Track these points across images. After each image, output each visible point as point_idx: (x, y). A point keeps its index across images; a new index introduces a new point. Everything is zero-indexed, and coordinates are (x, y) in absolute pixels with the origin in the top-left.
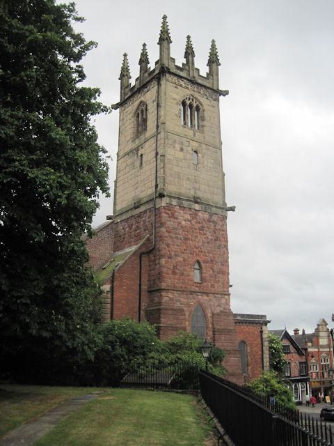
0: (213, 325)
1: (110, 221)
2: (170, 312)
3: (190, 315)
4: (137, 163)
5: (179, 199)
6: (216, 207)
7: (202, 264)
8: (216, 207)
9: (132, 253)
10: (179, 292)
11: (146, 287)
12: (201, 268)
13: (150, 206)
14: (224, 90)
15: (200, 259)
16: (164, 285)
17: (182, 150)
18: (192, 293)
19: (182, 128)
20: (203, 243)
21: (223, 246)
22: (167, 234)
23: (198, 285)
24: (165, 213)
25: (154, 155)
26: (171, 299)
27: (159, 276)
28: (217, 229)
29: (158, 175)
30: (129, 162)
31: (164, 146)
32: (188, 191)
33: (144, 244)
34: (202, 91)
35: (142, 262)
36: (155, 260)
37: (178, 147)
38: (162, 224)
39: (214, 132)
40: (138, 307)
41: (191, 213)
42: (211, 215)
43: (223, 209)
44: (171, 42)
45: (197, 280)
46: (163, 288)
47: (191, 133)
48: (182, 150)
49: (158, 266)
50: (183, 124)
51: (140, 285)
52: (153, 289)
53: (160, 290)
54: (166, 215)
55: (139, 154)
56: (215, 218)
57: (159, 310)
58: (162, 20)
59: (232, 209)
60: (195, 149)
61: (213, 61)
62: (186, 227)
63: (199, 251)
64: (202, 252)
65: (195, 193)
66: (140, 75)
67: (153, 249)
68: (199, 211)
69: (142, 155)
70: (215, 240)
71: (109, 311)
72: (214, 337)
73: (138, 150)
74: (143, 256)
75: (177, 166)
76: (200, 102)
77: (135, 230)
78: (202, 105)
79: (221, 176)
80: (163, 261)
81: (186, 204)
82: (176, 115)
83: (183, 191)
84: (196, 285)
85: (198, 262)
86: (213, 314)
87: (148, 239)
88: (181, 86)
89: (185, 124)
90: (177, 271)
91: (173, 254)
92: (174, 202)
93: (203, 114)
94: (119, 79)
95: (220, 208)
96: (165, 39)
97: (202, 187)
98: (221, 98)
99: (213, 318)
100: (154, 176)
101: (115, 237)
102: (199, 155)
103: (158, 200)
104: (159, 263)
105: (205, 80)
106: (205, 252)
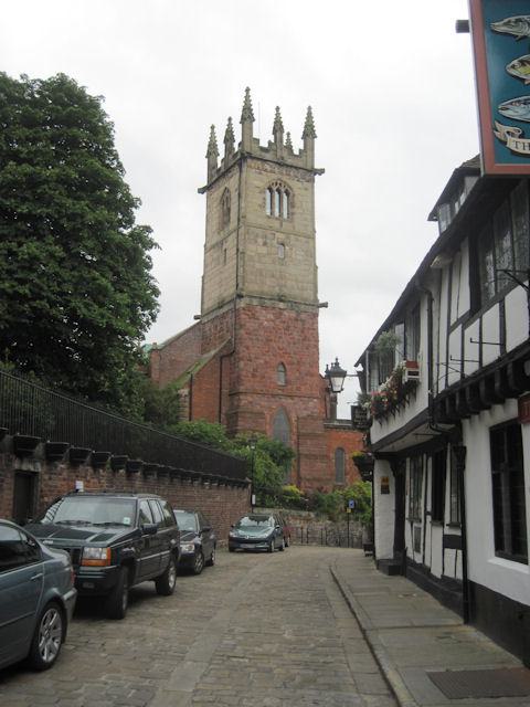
2: (248, 415)
4: (222, 260)
12: (285, 371)
13: (232, 306)
15: (283, 360)
16: (242, 389)
17: (265, 244)
18: (273, 396)
20: (289, 343)
22: (246, 336)
27: (238, 380)
30: (215, 255)
37: (260, 241)
42: (298, 313)
45: (281, 382)
47: (276, 224)
48: (265, 244)
53: (238, 393)
56: (303, 316)
59: (325, 305)
61: (309, 133)
80: (242, 364)
81: (268, 303)
83: (266, 289)
87: (230, 341)
88: (266, 170)
91: (253, 356)
92: (255, 302)
96: (247, 117)
98: (317, 177)
103: (238, 300)
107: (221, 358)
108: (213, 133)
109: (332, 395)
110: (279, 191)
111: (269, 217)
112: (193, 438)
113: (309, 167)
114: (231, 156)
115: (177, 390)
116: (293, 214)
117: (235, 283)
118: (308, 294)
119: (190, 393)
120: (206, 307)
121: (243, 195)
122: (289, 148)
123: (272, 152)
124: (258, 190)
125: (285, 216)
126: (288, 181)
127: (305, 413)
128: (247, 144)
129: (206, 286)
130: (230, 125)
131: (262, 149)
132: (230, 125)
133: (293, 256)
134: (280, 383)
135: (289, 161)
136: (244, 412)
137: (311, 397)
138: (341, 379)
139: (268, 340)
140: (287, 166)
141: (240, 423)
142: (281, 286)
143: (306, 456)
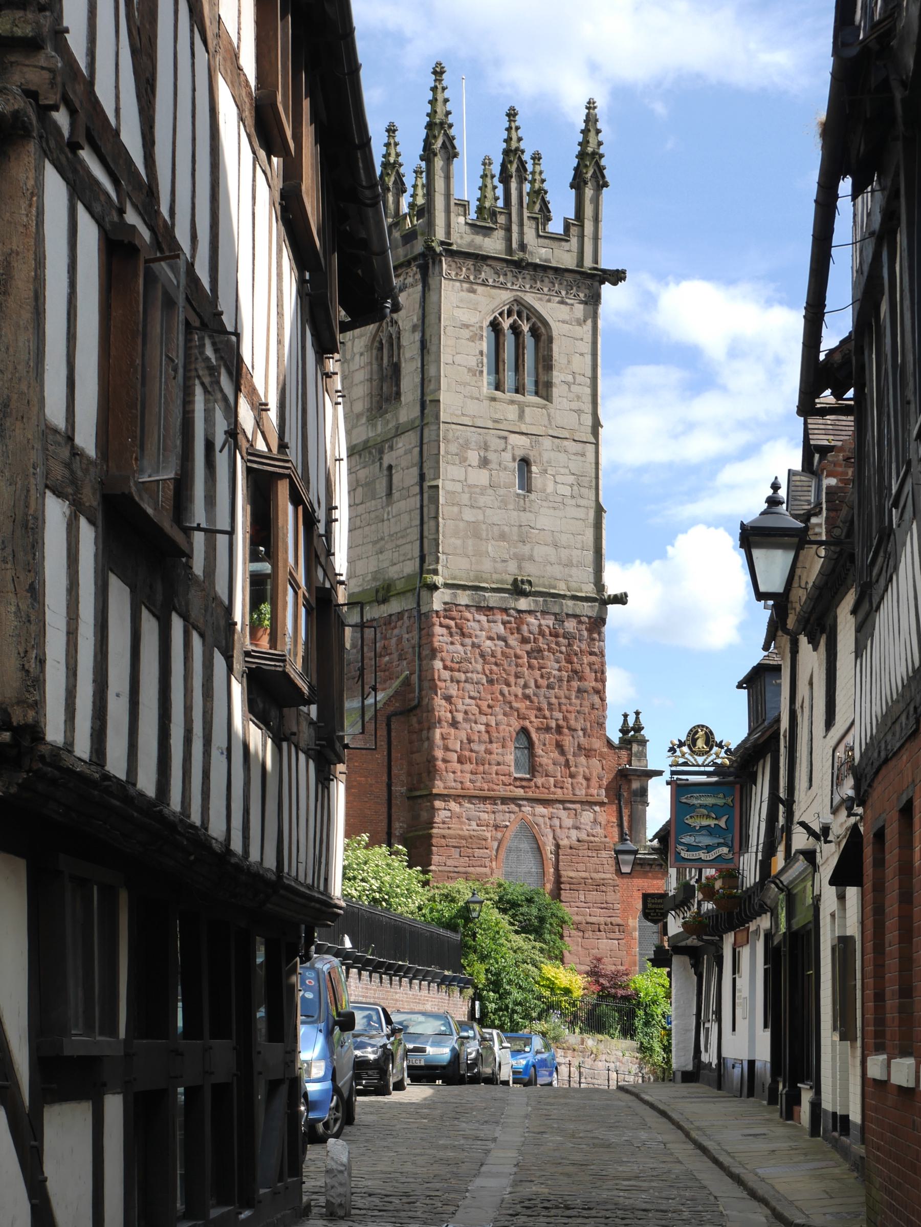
0: (557, 869)
4: (381, 486)
7: (534, 736)
8: (575, 598)
11: (404, 789)
14: (613, 267)
16: (439, 787)
17: (484, 463)
19: (486, 403)
22: (446, 674)
24: (441, 625)
25: (416, 479)
27: (429, 769)
29: (426, 533)
32: (499, 566)
35: (393, 734)
36: (421, 730)
37: (473, 457)
39: (578, 397)
41: (506, 618)
42: (559, 618)
44: (606, 185)
46: (435, 791)
48: (484, 463)
51: (389, 786)
52: (418, 793)
54: (444, 631)
55: (385, 465)
59: (621, 599)
60: (520, 453)
65: (520, 568)
67: (415, 707)
73: (381, 452)
74: (393, 719)
75: (472, 507)
78: (546, 324)
82: (469, 370)
86: (558, 846)
87: (407, 682)
91: (460, 717)
97: (540, 552)
98: (607, 289)
100: (414, 534)
104: (428, 739)
105: (555, 244)
109: (635, 785)
117: (417, 553)
124: (466, 333)
126: (538, 306)
135: (540, 252)
140: (536, 267)
142: (520, 559)
143: (578, 927)
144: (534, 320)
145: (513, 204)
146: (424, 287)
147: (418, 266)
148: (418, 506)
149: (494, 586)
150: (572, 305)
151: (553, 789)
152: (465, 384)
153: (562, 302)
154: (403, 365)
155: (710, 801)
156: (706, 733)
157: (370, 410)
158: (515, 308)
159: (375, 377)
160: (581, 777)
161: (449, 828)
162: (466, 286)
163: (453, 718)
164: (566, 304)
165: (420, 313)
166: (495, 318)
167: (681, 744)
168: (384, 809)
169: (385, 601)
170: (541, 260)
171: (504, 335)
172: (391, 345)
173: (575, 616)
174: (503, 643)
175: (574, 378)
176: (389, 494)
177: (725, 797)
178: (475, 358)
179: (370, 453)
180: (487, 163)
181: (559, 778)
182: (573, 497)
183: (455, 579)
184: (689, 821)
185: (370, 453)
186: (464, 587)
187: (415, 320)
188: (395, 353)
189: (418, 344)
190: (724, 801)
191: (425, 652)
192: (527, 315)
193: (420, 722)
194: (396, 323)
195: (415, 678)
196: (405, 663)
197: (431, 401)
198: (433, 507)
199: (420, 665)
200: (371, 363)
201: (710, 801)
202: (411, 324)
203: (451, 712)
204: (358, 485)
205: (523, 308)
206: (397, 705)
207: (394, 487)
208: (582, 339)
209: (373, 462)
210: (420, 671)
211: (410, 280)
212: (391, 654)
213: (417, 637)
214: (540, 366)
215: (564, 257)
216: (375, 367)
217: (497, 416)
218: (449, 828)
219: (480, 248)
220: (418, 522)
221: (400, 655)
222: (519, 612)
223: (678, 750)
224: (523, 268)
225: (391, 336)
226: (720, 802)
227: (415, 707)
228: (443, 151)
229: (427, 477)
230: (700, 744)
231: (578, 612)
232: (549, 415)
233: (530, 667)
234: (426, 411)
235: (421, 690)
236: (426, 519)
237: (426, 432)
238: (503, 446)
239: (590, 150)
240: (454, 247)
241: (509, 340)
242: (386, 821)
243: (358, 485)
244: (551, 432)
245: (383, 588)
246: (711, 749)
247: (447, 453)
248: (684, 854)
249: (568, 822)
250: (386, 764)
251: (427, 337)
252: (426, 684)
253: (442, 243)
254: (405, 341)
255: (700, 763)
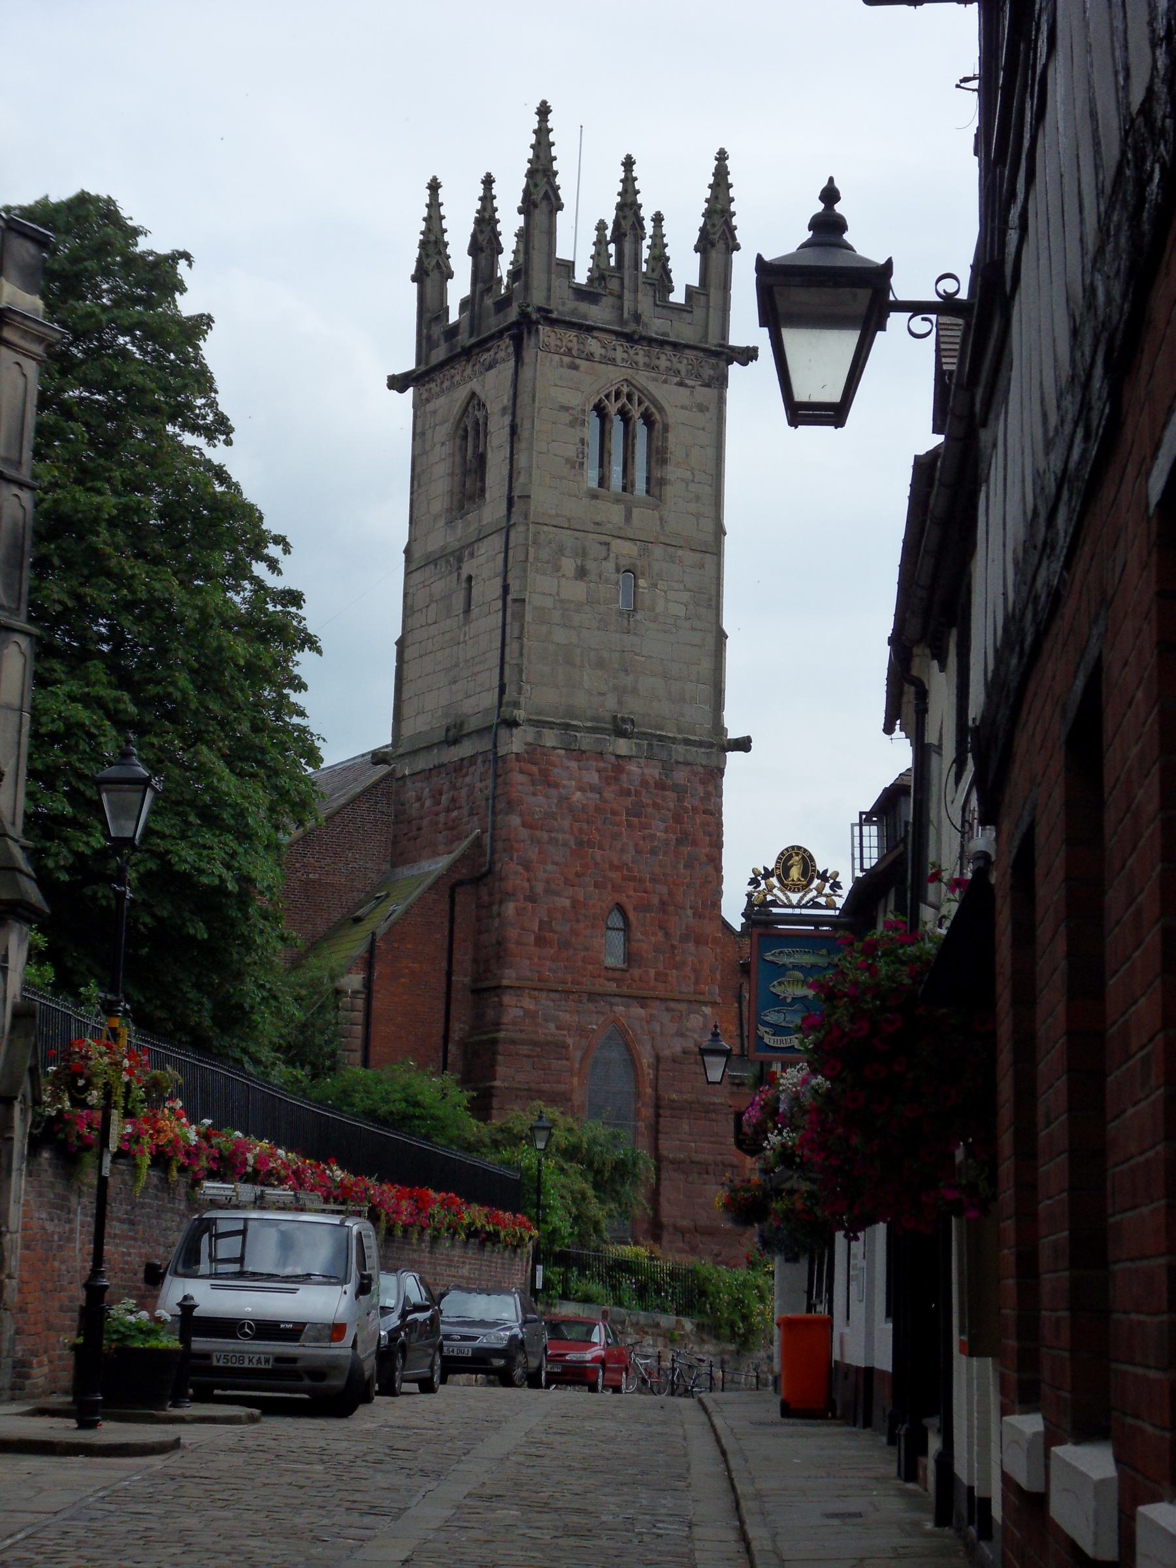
0: (656, 1089)
1: (383, 770)
2: (525, 1049)
3: (583, 1059)
5: (567, 727)
6: (687, 742)
7: (632, 915)
8: (687, 742)
9: (429, 881)
10: (552, 995)
11: (467, 980)
12: (627, 928)
13: (484, 745)
14: (743, 344)
15: (623, 899)
16: (509, 977)
17: (582, 573)
18: (593, 996)
20: (638, 852)
21: (704, 859)
22: (524, 833)
23: (617, 974)
24: (521, 772)
25: (498, 592)
26: (532, 1015)
28: (686, 810)
29: (507, 658)
30: (439, 587)
31: (525, 571)
33: (464, 857)
34: (663, 363)
35: (457, 909)
36: (491, 904)
37: (569, 565)
38: (511, 805)
39: (698, 498)
40: (442, 1032)
41: (602, 765)
42: (668, 767)
43: (711, 745)
44: (737, 247)
45: (614, 959)
46: (505, 982)
47: (614, 514)
48: (582, 573)
49: (496, 923)
50: (594, 484)
51: (449, 974)
52: (484, 985)
53: (498, 989)
55: (464, 576)
56: (680, 776)
57: (495, 1042)
58: (534, 122)
59: (744, 745)
60: (625, 562)
62: (584, 808)
63: (624, 878)
64: (633, 879)
65: (620, 703)
66: (473, 291)
67: (484, 875)
68: (630, 757)
69: (470, 578)
70: (679, 842)
71: (358, 1043)
72: (657, 1123)
73: (460, 560)
76: (654, 402)
77: (448, 810)
78: (661, 409)
79: (711, 640)
80: (510, 908)
81: (586, 741)
82: (568, 461)
83: (580, 700)
84: (610, 974)
85: (620, 908)
86: (658, 1058)
87: (478, 843)
88: (590, 357)
89: (603, 481)
90: (548, 935)
91: (540, 888)
92: (550, 739)
93: (665, 439)
94: (414, 279)
95: (700, 744)
98: (734, 369)
99: (657, 1069)
101: (396, 823)
102: (642, 582)
103: (503, 732)
104: (499, 914)
106: (641, 881)
107: (453, 889)
108: (434, 205)
110: (624, 414)
111: (594, 496)
112: (383, 1122)
113: (712, 342)
114: (489, 302)
115: (333, 978)
116: (662, 482)
117: (496, 682)
118: (695, 715)
119: (368, 984)
120: (408, 730)
121: (524, 434)
122: (662, 279)
123: (607, 301)
124: (566, 417)
125: (640, 485)
126: (652, 387)
127: (677, 1046)
128: (538, 277)
129: (410, 673)
130: (487, 198)
131: (581, 293)
132: (487, 198)
133: (660, 608)
134: (610, 961)
135: (656, 326)
136: (513, 1042)
137: (695, 1002)
138: (845, 342)
139: (580, 844)
140: (651, 341)
141: (501, 1070)
144: (647, 404)
145: (626, 266)
146: (517, 362)
147: (512, 337)
148: (500, 624)
149: (589, 724)
150: (693, 387)
151: (652, 983)
152: (561, 478)
153: (681, 384)
154: (489, 455)
155: (807, 959)
156: (803, 858)
157: (450, 510)
158: (625, 390)
159: (457, 471)
160: (688, 969)
161: (521, 1031)
162: (567, 359)
163: (531, 888)
164: (686, 386)
165: (511, 392)
166: (600, 400)
167: (768, 874)
168: (441, 1005)
169: (456, 741)
170: (657, 333)
171: (611, 422)
172: (478, 432)
173: (687, 764)
174: (597, 796)
175: (693, 474)
176: (467, 610)
177: (829, 953)
178: (574, 448)
179: (448, 562)
180: (601, 226)
181: (661, 969)
182: (687, 619)
183: (540, 714)
184: (777, 990)
185: (448, 562)
186: (551, 725)
187: (505, 401)
188: (482, 442)
189: (507, 430)
190: (828, 960)
191: (501, 806)
192: (639, 398)
193: (491, 894)
194: (484, 405)
195: (487, 839)
196: (476, 818)
197: (519, 497)
198: (516, 625)
199: (494, 822)
200: (453, 455)
201: (807, 959)
202: (501, 406)
203: (528, 880)
204: (431, 601)
205: (634, 390)
206: (464, 871)
207: (473, 602)
208: (703, 429)
209: (451, 572)
210: (494, 828)
211: (502, 354)
212: (460, 808)
213: (491, 786)
214: (654, 459)
215: (685, 332)
216: (458, 459)
217: (598, 518)
218: (521, 1031)
219: (585, 317)
220: (499, 645)
221: (472, 809)
222: (618, 756)
223: (763, 882)
224: (636, 342)
225: (477, 423)
226: (822, 961)
227: (484, 875)
228: (544, 203)
229: (512, 589)
230: (795, 873)
231: (690, 759)
232: (661, 519)
233: (630, 825)
234: (514, 510)
235: (493, 852)
236: (508, 640)
237: (513, 534)
238: (604, 554)
239: (719, 206)
240: (554, 315)
241: (617, 427)
242: (443, 1020)
243: (431, 601)
244: (662, 539)
245: (455, 726)
246: (810, 882)
247: (537, 559)
248: (769, 1040)
249: (672, 1028)
250: (446, 946)
251: (518, 420)
252: (500, 845)
253: (540, 309)
254: (492, 427)
255: (795, 902)
